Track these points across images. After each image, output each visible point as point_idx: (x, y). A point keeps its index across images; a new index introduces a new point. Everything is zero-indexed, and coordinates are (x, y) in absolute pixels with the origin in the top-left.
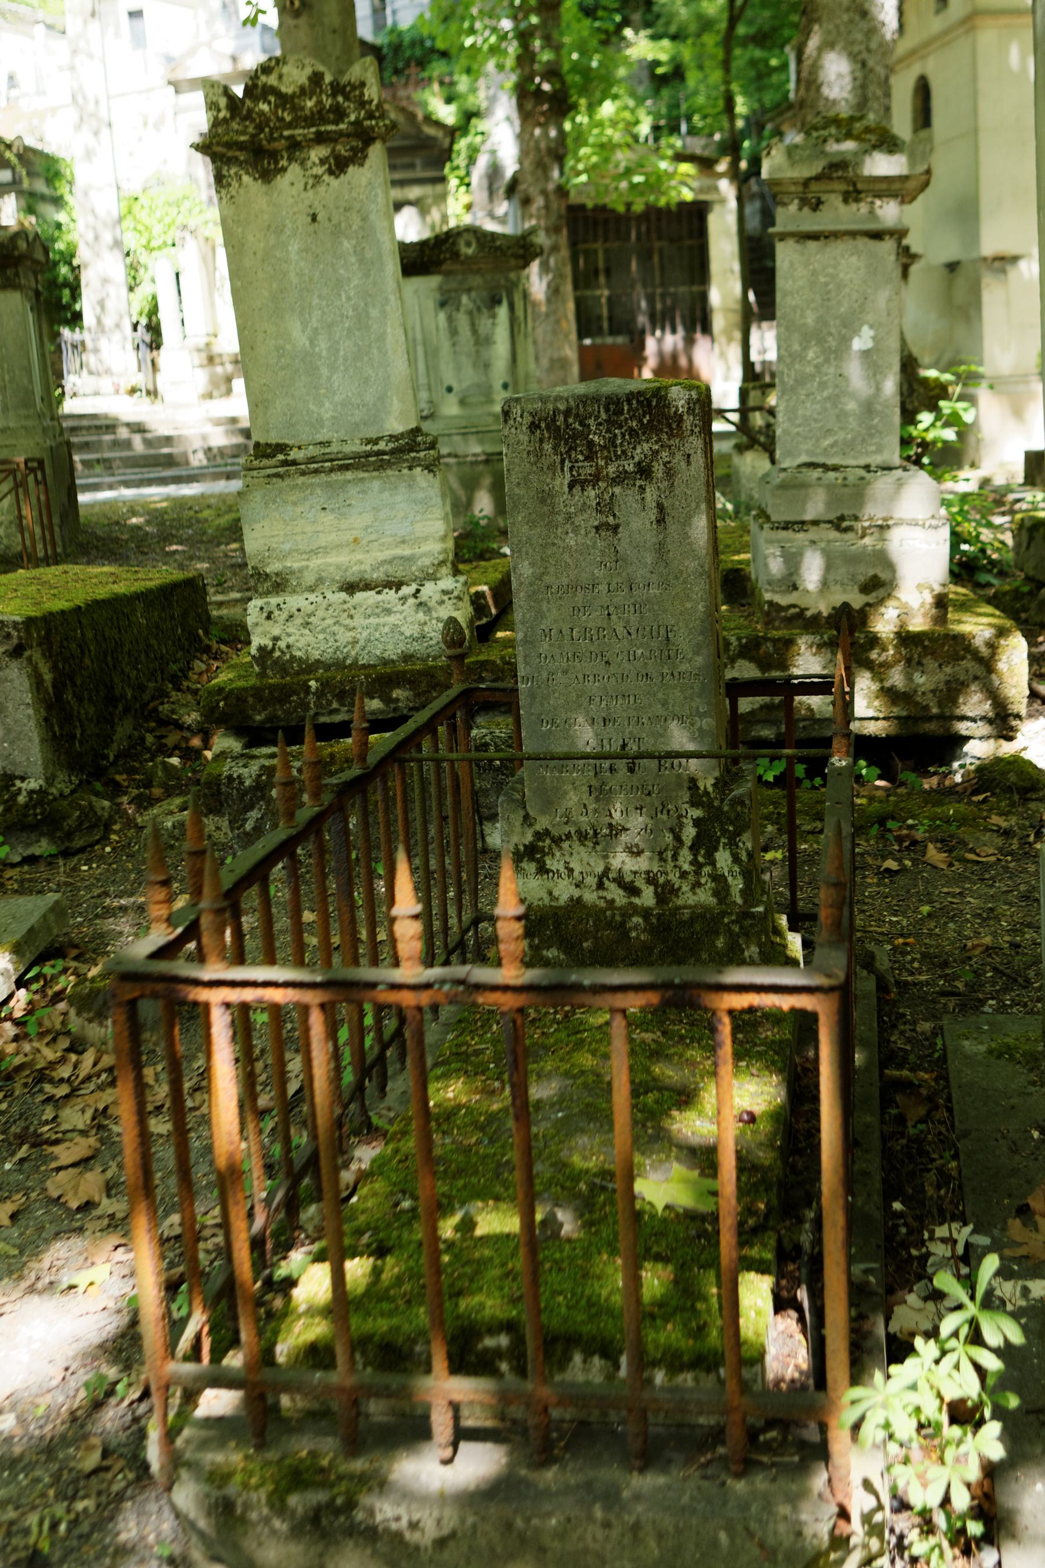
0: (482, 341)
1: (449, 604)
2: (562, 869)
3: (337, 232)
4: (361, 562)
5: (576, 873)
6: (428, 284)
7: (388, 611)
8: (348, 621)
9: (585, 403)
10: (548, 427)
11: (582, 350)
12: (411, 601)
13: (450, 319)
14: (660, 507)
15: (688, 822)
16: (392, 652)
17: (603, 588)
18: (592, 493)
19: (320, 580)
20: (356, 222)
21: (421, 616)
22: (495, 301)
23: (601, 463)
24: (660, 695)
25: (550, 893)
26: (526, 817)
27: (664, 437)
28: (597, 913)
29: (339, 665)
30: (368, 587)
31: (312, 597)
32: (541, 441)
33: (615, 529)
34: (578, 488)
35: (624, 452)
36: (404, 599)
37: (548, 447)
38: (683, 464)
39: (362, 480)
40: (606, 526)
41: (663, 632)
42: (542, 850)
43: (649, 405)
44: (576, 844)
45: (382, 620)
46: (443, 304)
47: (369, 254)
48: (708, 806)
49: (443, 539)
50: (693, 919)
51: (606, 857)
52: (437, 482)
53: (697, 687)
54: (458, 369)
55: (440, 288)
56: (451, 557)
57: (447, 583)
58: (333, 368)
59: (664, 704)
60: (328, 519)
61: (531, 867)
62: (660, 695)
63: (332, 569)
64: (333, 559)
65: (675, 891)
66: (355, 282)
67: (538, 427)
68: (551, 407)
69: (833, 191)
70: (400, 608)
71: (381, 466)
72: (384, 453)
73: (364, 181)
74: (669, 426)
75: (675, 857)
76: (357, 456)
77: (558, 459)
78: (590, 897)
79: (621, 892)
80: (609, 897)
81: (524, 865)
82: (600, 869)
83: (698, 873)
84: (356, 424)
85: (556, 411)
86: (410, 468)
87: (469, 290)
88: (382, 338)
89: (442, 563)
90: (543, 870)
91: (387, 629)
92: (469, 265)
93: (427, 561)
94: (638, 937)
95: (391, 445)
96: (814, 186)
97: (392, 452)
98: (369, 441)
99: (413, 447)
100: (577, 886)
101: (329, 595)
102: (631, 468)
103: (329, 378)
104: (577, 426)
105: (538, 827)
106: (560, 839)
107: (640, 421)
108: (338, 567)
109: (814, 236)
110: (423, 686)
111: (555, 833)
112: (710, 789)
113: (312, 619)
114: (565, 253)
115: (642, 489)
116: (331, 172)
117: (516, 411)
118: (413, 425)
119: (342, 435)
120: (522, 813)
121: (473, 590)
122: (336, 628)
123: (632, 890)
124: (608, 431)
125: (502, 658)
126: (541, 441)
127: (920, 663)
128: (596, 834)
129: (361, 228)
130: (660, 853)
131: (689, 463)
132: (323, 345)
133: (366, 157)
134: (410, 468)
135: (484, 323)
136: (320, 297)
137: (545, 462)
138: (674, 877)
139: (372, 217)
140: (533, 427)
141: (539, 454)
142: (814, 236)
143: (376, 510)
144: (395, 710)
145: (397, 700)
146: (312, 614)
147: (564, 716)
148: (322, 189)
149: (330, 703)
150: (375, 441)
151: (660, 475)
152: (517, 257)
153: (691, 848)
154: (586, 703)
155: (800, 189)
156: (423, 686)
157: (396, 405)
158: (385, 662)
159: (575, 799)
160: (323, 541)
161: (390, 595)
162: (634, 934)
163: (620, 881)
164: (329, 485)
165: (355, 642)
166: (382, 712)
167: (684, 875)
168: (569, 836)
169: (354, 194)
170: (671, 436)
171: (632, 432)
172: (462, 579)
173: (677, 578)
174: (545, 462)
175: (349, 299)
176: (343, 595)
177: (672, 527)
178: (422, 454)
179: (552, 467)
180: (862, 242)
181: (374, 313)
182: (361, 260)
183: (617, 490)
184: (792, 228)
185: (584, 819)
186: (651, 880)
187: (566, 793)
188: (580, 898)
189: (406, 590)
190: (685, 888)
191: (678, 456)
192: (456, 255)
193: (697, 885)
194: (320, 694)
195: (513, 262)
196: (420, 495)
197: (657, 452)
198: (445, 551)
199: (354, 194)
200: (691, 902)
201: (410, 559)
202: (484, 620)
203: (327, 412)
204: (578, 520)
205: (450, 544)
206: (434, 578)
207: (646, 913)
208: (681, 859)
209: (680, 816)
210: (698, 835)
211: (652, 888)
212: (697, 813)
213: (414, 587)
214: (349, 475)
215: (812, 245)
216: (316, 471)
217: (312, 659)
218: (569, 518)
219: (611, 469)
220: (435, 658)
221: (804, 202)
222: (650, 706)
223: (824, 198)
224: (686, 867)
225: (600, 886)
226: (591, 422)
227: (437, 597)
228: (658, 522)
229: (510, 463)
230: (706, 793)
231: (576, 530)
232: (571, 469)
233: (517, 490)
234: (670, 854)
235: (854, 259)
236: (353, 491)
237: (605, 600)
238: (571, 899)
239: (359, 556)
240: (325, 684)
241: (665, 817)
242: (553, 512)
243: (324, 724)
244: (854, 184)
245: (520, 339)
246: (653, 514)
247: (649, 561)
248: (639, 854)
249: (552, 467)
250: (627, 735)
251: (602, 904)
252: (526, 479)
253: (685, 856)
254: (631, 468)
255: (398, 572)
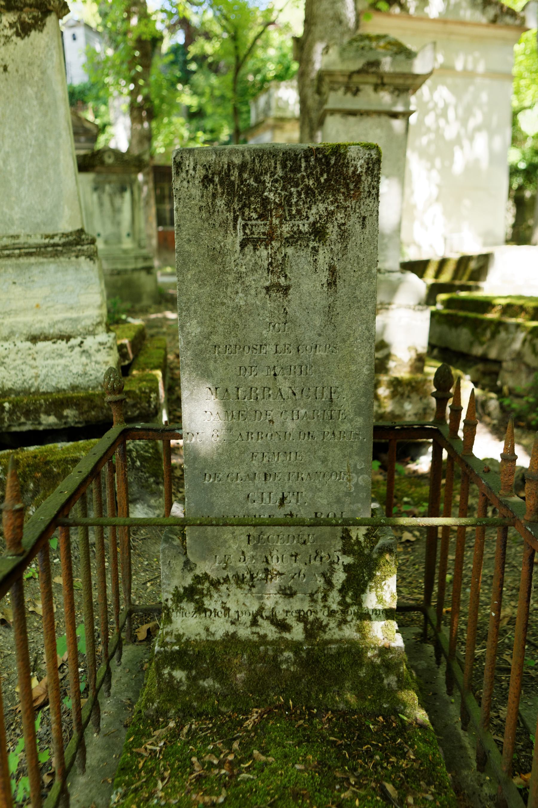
0: (116, 211)
1: (104, 352)
2: (219, 608)
3: (23, 81)
4: (41, 321)
5: (232, 612)
6: (88, 178)
7: (61, 356)
8: (32, 362)
9: (261, 158)
10: (221, 182)
11: (159, 233)
12: (77, 349)
13: (99, 198)
14: (332, 270)
15: (339, 568)
16: (64, 384)
17: (271, 349)
18: (263, 252)
19: (12, 333)
20: (37, 75)
21: (84, 359)
22: (123, 189)
23: (276, 221)
24: (320, 453)
25: (207, 629)
26: (187, 563)
27: (341, 197)
28: (246, 644)
29: (26, 392)
30: (46, 338)
31: (6, 345)
32: (214, 196)
33: (286, 290)
34: (250, 247)
35: (299, 212)
36: (72, 348)
37: (220, 203)
38: (358, 227)
39: (42, 264)
40: (277, 287)
41: (326, 393)
42: (201, 592)
43: (328, 163)
44: (233, 588)
45: (57, 362)
46: (96, 189)
47: (46, 100)
48: (359, 554)
49: (100, 307)
50: (339, 654)
51: (261, 598)
52: (96, 267)
53: (356, 445)
54: (103, 224)
55: (95, 181)
56: (105, 320)
57: (103, 337)
58: (21, 182)
59: (324, 461)
60: (18, 290)
61: (190, 607)
62: (320, 453)
63: (21, 326)
64: (21, 319)
65: (323, 628)
66: (37, 119)
67: (212, 181)
68: (225, 160)
69: (366, 83)
70: (69, 353)
71: (56, 254)
72: (58, 245)
73: (43, 43)
74: (347, 186)
75: (325, 598)
76: (38, 246)
77: (231, 216)
78: (244, 632)
79: (273, 628)
80: (262, 632)
81: (184, 605)
82: (254, 608)
83: (344, 612)
84: (38, 224)
85: (230, 165)
86: (77, 257)
87: (110, 183)
88: (56, 162)
89: (99, 324)
90: (201, 609)
91: (60, 368)
92: (110, 169)
93: (88, 322)
94: (288, 669)
95: (63, 240)
96: (356, 79)
97: (64, 245)
98: (47, 237)
99: (78, 242)
100: (233, 623)
101: (18, 343)
102: (305, 228)
103: (18, 190)
104: (252, 182)
105: (198, 572)
106: (219, 582)
107: (318, 180)
108: (25, 324)
109: (352, 113)
110: (85, 407)
111: (213, 576)
112: (362, 539)
113: (6, 360)
114: (151, 185)
115: (315, 250)
116: (18, 34)
117: (189, 163)
118: (79, 227)
119: (28, 231)
120: (182, 559)
121: (119, 342)
122: (23, 367)
123: (283, 626)
124: (284, 188)
125: (140, 389)
126: (214, 196)
127: (409, 397)
128: (252, 577)
129: (42, 79)
130: (312, 595)
131: (364, 226)
132: (13, 165)
133: (44, 25)
134: (77, 257)
135: (117, 201)
136: (11, 129)
137: (218, 219)
138: (323, 616)
139: (49, 71)
140: (207, 180)
141: (211, 210)
142: (352, 113)
143: (52, 285)
144: (65, 423)
145: (67, 417)
146: (7, 356)
147: (227, 471)
148: (11, 46)
149: (19, 418)
150: (52, 237)
151: (334, 237)
152: (135, 166)
153: (340, 591)
154: (248, 459)
155: (345, 79)
156: (85, 407)
157: (67, 212)
158: (59, 391)
159: (235, 547)
160: (14, 305)
161: (62, 345)
162: (284, 666)
163: (273, 620)
164: (18, 266)
165: (37, 376)
166: (56, 424)
167: (332, 613)
168: (226, 580)
169: (35, 53)
170: (347, 197)
171: (308, 190)
172: (112, 335)
173: (344, 341)
174: (218, 219)
175: (32, 132)
176: (29, 344)
177: (342, 289)
178: (85, 247)
179: (224, 224)
180: (384, 119)
181: (51, 144)
182: (41, 104)
183: (290, 251)
184: (339, 106)
185: (242, 564)
186: (301, 618)
187: (225, 541)
188: (235, 633)
189: (73, 342)
190: (332, 625)
191: (354, 218)
192: (102, 163)
193: (344, 621)
194: (12, 412)
195: (133, 169)
196: (84, 276)
197: (332, 213)
198: (101, 315)
199: (35, 53)
200: (336, 637)
201: (76, 321)
202: (127, 362)
203: (16, 214)
204: (249, 280)
205: (104, 311)
206: (93, 333)
207: (296, 647)
208: (330, 600)
209: (333, 562)
210: (348, 580)
211: (301, 625)
212: (348, 560)
213: (79, 339)
214: (33, 260)
215: (352, 120)
216: (8, 256)
217: (6, 388)
218: (240, 277)
219: (286, 229)
220: (93, 388)
221: (348, 89)
222: (310, 462)
223: (361, 87)
224: (335, 607)
225: (254, 623)
226: (267, 178)
227: (95, 347)
228: (329, 284)
229: (180, 218)
230: (358, 542)
231: (246, 290)
232: (244, 227)
233: (187, 247)
234: (320, 595)
235: (378, 131)
236: (35, 271)
237: (271, 360)
238: (227, 634)
239: (40, 317)
240: (15, 405)
241: (318, 563)
242: (224, 271)
243: (16, 433)
244: (382, 78)
245: (136, 211)
246: (324, 277)
247: (318, 323)
248: (292, 595)
249: (224, 224)
250: (286, 489)
251: (255, 638)
252: (197, 236)
253: (335, 597)
254: (305, 228)
255: (66, 328)
